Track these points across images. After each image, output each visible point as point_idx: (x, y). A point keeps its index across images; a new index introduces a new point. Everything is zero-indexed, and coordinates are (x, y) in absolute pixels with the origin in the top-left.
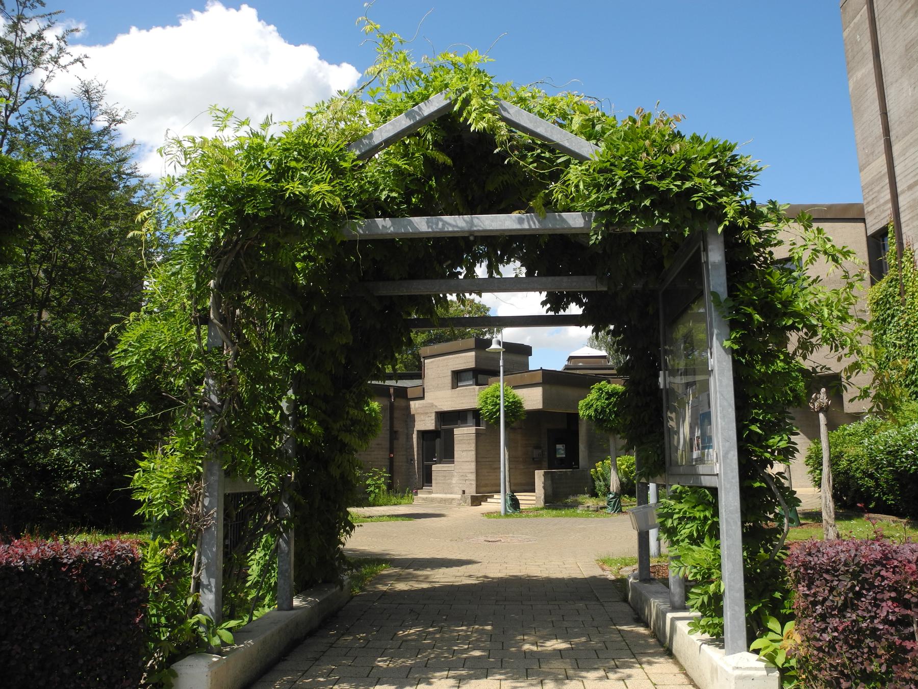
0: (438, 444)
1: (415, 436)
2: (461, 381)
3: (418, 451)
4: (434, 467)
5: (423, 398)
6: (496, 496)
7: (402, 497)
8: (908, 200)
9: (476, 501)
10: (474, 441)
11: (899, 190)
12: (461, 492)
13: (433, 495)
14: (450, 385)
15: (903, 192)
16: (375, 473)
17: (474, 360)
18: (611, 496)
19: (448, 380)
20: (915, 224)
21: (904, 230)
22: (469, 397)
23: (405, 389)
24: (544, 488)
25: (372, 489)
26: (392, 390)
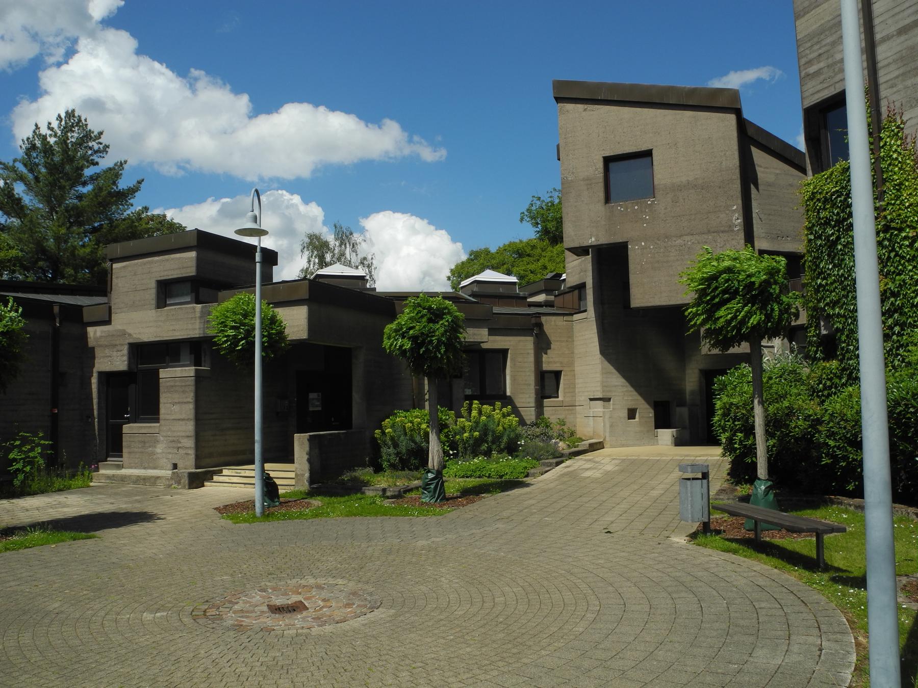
0: (134, 391)
1: (94, 381)
2: (171, 297)
3: (99, 403)
4: (126, 428)
5: (108, 322)
6: (225, 472)
7: (73, 476)
8: (899, 48)
9: (196, 481)
10: (193, 388)
11: (878, 37)
12: (170, 466)
13: (124, 472)
14: (154, 302)
15: (887, 38)
16: (25, 441)
17: (194, 263)
18: (430, 476)
19: (151, 294)
20: (909, 83)
21: (884, 92)
22: (184, 322)
23: (79, 308)
24: (309, 461)
25: (19, 466)
26: (56, 309)
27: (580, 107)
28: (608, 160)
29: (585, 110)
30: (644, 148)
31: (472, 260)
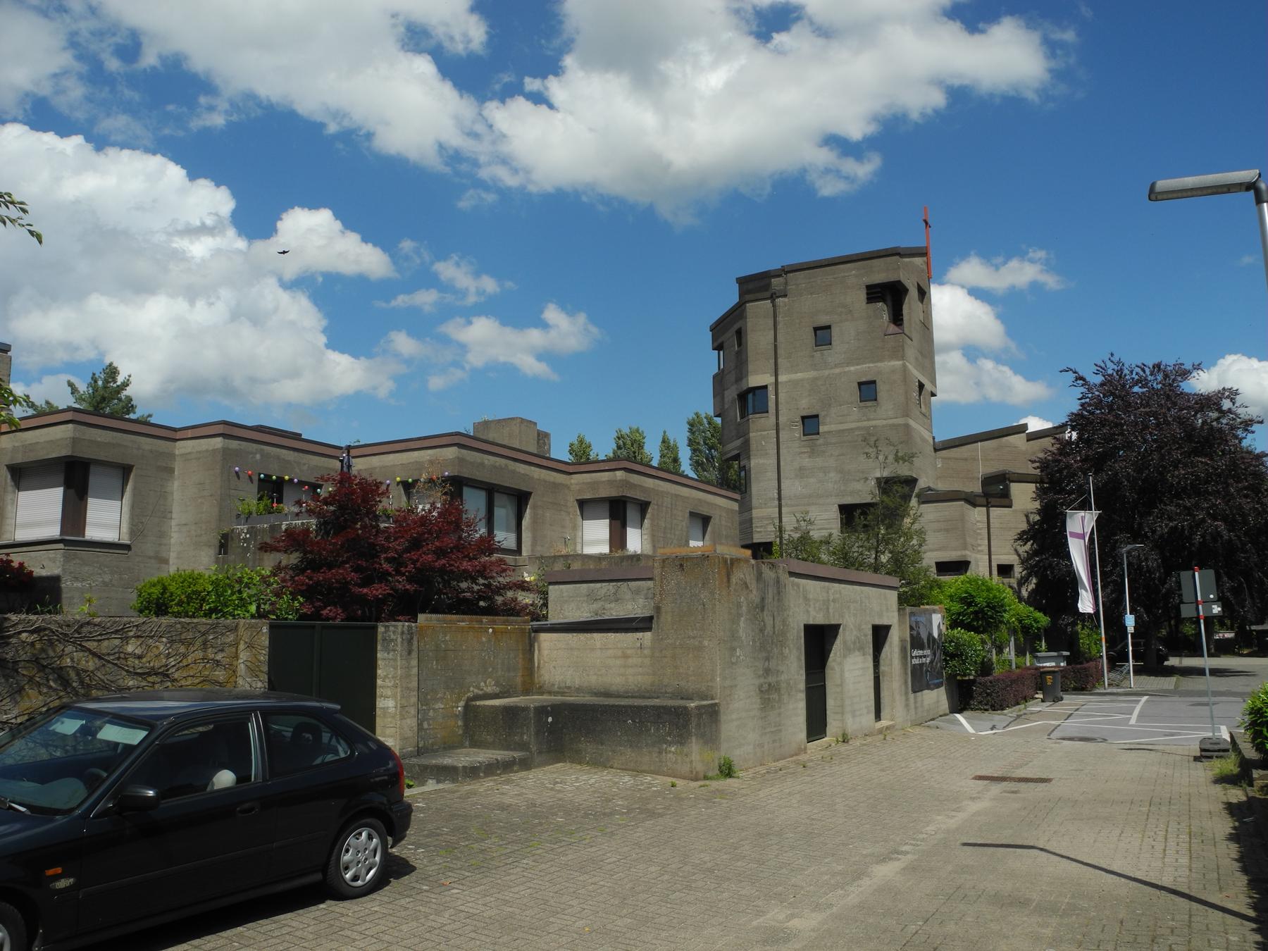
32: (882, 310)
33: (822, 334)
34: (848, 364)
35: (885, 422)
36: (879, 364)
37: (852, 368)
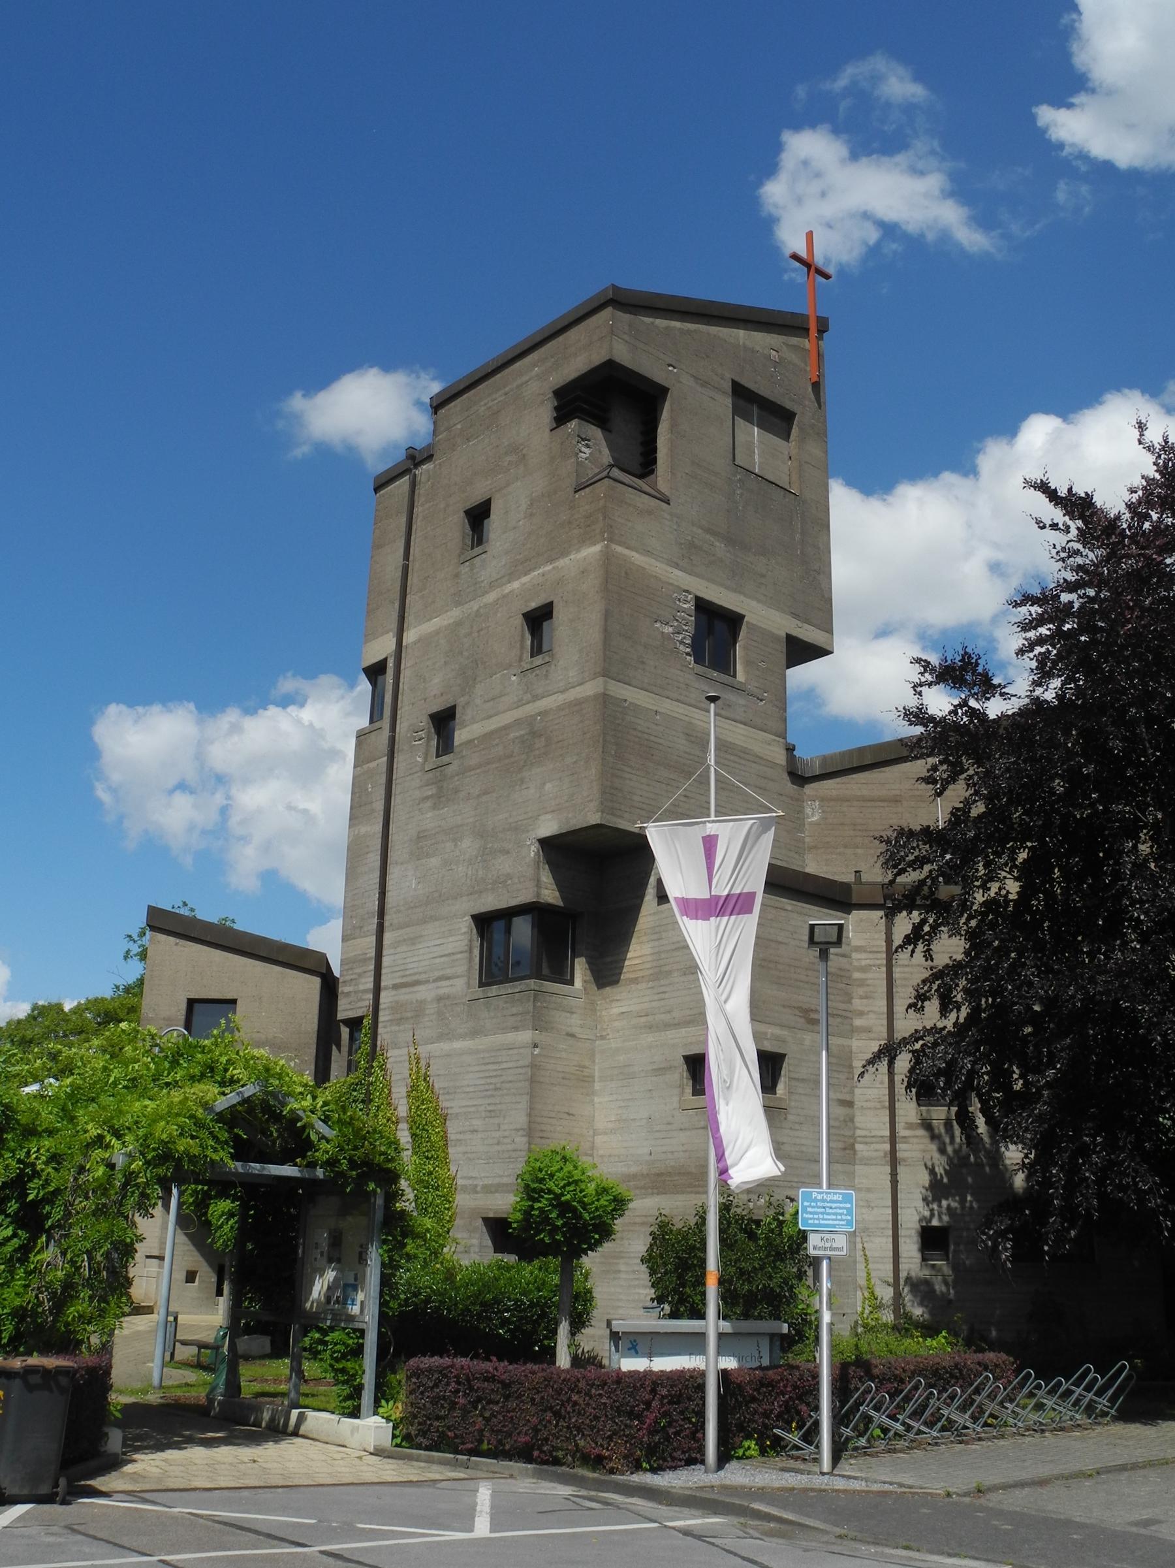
27: (172, 939)
28: (191, 1003)
29: (177, 944)
30: (229, 996)
31: (35, 1018)
32: (592, 447)
33: (478, 516)
34: (512, 576)
35: (560, 698)
36: (562, 563)
37: (516, 585)
